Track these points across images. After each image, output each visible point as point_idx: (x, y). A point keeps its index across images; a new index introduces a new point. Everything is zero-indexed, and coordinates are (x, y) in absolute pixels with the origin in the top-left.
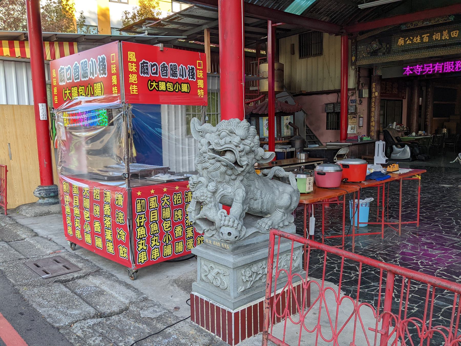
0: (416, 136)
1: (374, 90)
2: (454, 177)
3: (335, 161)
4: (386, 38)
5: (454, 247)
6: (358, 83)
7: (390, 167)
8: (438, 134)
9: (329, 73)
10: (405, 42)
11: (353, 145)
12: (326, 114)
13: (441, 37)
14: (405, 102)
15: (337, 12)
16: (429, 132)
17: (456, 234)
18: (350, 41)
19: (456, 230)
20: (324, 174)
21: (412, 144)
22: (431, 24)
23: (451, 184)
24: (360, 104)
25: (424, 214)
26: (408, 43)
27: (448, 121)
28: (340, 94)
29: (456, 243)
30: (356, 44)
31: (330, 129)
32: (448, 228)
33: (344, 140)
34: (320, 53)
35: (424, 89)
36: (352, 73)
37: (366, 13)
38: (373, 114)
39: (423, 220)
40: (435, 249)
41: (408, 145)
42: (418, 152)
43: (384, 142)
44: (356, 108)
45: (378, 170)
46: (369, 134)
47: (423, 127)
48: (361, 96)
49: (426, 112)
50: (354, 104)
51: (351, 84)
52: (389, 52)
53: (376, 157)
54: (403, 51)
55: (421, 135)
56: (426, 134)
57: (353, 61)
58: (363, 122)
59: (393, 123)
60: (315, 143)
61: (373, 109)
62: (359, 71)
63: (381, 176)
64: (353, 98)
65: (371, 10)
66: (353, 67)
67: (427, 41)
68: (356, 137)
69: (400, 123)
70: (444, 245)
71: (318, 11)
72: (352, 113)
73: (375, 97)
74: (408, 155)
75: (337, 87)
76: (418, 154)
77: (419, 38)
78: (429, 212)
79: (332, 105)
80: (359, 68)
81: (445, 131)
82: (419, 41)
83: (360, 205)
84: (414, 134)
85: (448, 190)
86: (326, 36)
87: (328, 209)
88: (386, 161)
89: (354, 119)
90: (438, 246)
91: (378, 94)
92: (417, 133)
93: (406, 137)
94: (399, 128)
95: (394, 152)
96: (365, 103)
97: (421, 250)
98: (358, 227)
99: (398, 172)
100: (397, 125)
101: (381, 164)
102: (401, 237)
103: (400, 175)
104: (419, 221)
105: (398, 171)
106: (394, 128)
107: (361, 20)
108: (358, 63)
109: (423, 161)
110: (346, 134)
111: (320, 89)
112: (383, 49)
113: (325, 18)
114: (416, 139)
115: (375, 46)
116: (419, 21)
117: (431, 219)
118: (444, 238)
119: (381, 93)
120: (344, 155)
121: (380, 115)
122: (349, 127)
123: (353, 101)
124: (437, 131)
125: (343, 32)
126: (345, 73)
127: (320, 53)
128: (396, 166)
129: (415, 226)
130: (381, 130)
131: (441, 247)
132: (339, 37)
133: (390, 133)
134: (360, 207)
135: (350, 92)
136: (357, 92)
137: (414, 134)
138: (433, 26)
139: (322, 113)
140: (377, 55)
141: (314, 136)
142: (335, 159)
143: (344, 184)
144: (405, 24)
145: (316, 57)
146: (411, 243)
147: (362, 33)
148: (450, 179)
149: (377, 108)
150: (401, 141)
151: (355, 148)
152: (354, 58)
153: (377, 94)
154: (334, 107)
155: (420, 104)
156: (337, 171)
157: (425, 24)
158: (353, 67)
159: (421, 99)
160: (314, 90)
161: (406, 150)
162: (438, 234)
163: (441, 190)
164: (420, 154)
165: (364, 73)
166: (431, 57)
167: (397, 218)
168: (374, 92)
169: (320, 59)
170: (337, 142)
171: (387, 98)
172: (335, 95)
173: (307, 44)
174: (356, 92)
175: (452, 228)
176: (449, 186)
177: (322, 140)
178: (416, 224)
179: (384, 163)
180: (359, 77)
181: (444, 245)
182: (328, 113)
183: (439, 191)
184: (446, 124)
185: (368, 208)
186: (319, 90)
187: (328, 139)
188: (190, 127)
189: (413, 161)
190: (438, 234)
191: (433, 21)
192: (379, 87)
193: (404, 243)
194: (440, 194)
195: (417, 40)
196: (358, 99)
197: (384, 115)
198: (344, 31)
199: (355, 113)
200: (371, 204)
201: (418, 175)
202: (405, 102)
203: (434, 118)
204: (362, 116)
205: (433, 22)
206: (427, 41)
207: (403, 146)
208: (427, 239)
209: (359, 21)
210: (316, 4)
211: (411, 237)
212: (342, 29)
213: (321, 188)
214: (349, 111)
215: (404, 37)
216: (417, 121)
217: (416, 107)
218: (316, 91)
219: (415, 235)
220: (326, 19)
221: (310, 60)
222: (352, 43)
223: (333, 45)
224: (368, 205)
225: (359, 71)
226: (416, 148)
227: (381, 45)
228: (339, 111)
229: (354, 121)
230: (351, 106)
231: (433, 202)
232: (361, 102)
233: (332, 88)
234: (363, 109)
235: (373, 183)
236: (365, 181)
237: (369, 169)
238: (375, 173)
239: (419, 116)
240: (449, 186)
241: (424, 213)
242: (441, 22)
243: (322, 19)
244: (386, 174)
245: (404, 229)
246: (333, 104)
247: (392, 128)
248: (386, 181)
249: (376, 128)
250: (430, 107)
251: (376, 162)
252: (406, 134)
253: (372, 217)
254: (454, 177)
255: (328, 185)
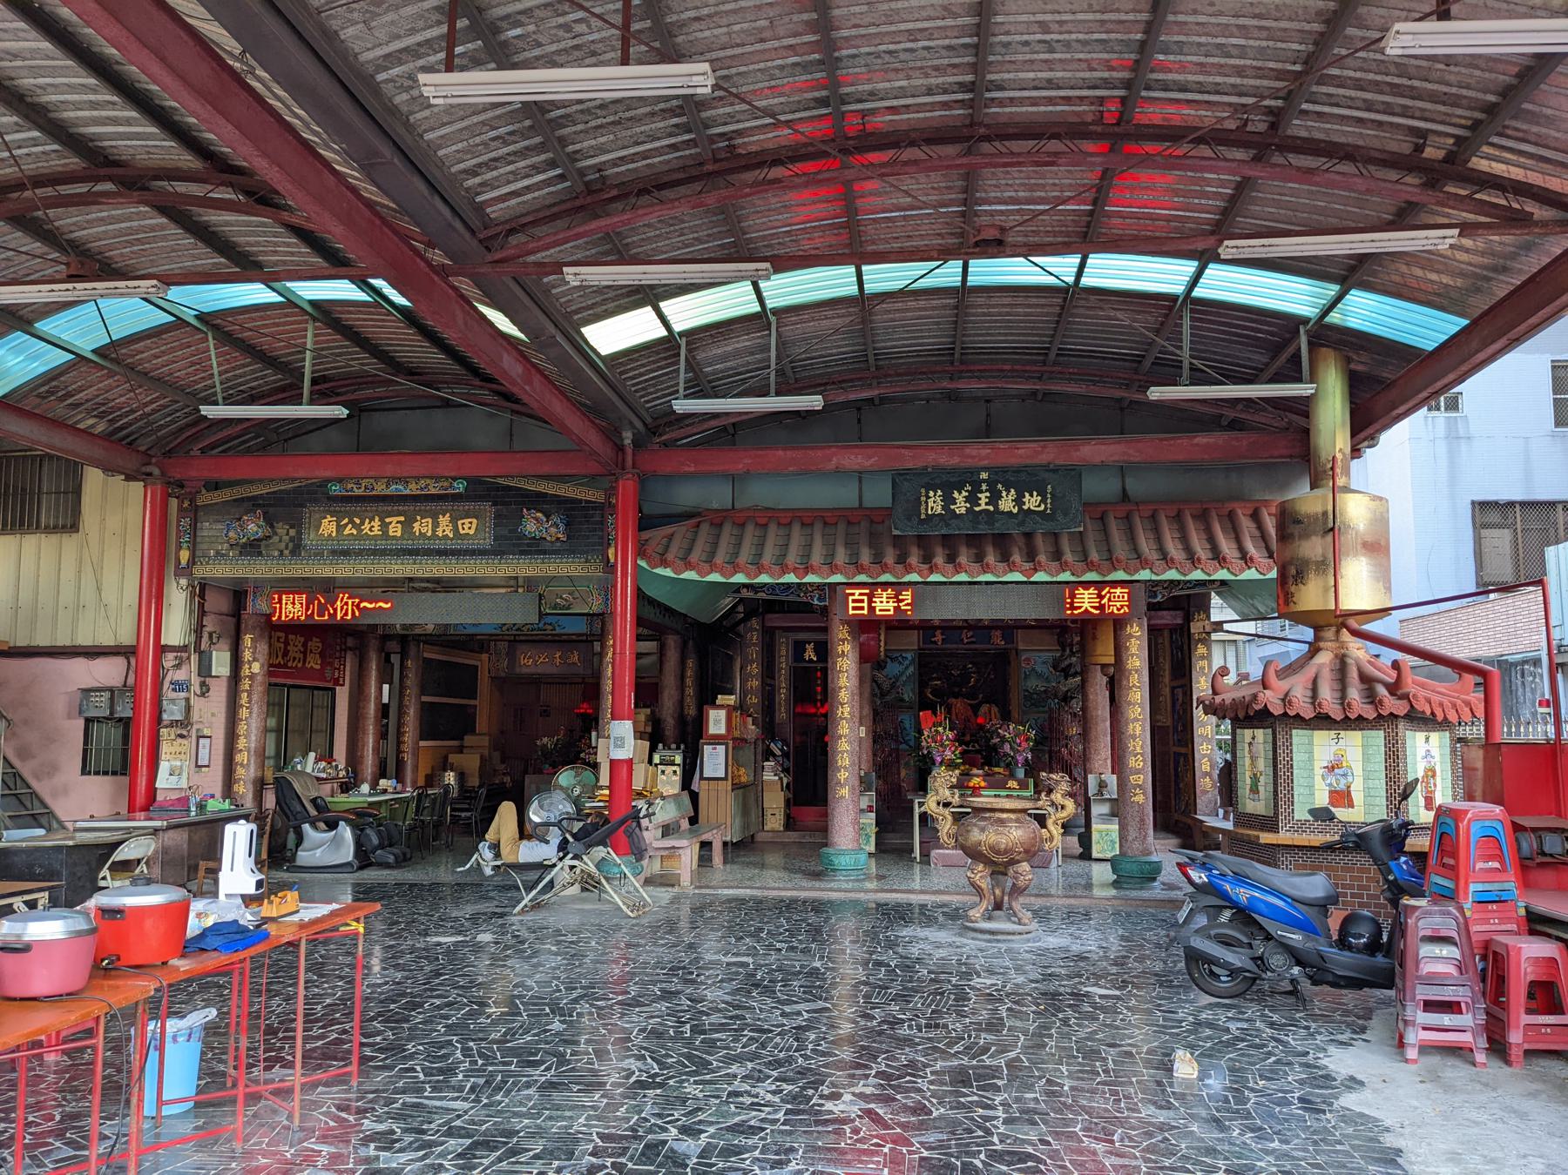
0: (370, 795)
1: (247, 655)
2: (469, 909)
3: (102, 884)
4: (287, 509)
5: (450, 1133)
6: (198, 630)
7: (271, 902)
8: (432, 786)
9: (99, 589)
10: (340, 528)
11: (169, 828)
12: (81, 722)
13: (434, 531)
14: (343, 695)
15: (133, 411)
16: (409, 781)
17: (460, 1089)
18: (174, 503)
19: (460, 1077)
20: (26, 948)
21: (360, 819)
22: (407, 492)
23: (459, 933)
24: (203, 695)
25: (378, 1039)
26: (346, 532)
27: (460, 750)
28: (133, 661)
29: (459, 1117)
30: (194, 513)
31: (97, 773)
32: (441, 1071)
33: (142, 810)
34: (70, 524)
35: (395, 659)
36: (177, 600)
37: (225, 433)
38: (242, 728)
39: (372, 1058)
40: (401, 1150)
41: (347, 821)
42: (375, 841)
43: (254, 826)
44: (188, 708)
45: (229, 918)
46: (228, 791)
47: (391, 766)
48: (205, 670)
49: (400, 725)
50: (183, 695)
51: (175, 629)
52: (296, 548)
53: (224, 876)
54: (333, 552)
55: (385, 791)
56: (399, 787)
57: (184, 562)
58: (211, 751)
59: (304, 756)
60: (34, 821)
61: (244, 713)
62: (202, 596)
63: (238, 936)
64: (180, 675)
65: (240, 427)
66: (184, 582)
67: (399, 534)
68: (184, 801)
69: (327, 756)
70: (423, 1132)
71: (69, 395)
72: (173, 724)
73: (252, 677)
74: (347, 853)
75: (126, 637)
76: (377, 848)
77: (376, 523)
78: (392, 1029)
79: (107, 695)
80: (203, 587)
81: (450, 778)
82: (377, 531)
83: (168, 1039)
84: (365, 788)
85: (451, 952)
86: (93, 478)
87: (57, 1063)
88: (259, 884)
89: (180, 740)
90: (408, 1139)
91: (262, 666)
92: (374, 785)
93: (342, 798)
94: (324, 770)
95: (305, 844)
96: (219, 692)
97: (359, 1161)
98: (157, 1119)
99: (295, 918)
100: (317, 760)
101: (243, 896)
102: (302, 1129)
103: (303, 926)
104: (360, 1064)
105: (299, 912)
106: (309, 770)
107: (213, 446)
108: (201, 571)
109: (387, 866)
110: (152, 791)
111: (63, 640)
112: (276, 539)
113: (91, 422)
114: (371, 804)
115: (253, 528)
116: (376, 479)
117: (394, 1049)
118: (426, 1106)
119: (271, 665)
120: (139, 861)
121: (266, 730)
122: (164, 767)
123: (178, 686)
124: (430, 780)
125: (150, 474)
126: (154, 596)
127: (70, 524)
128: (292, 896)
129: (345, 1082)
130: (269, 775)
131: (417, 1140)
132: (137, 487)
133: (296, 786)
134: (169, 1047)
135: (171, 656)
136: (194, 658)
137: (365, 788)
138: (414, 498)
139: (69, 717)
140: (260, 554)
141: (34, 795)
142: (104, 878)
143: (105, 977)
144: (340, 481)
145: (54, 538)
146: (331, 1144)
147: (216, 486)
148: (456, 919)
149: (255, 709)
150: (329, 811)
151: (179, 838)
152: (185, 556)
153: (256, 668)
154: (112, 699)
155: (385, 700)
156: (79, 934)
157: (394, 489)
158: (184, 582)
159: (386, 687)
160: (42, 641)
161: (343, 838)
162: (410, 1099)
163: (429, 954)
164: (381, 846)
165: (217, 602)
166: (411, 579)
167: (291, 1065)
168: (250, 663)
169: (69, 542)
170: (116, 816)
171: (289, 682)
172: (120, 662)
173: (24, 490)
174: (189, 658)
175: (450, 1071)
176: (453, 939)
177: (64, 809)
178: (349, 1074)
179: (251, 889)
180: (202, 613)
181: (423, 1132)
182: (88, 721)
183: (426, 958)
184: (453, 758)
185: (196, 1046)
186: (59, 644)
187: (84, 805)
188: (270, 580)
189: (361, 868)
190: (410, 1099)
191: (413, 486)
192: (263, 647)
193: (307, 1149)
194: (428, 969)
195: (372, 527)
196: (195, 681)
197: (278, 731)
198: (156, 471)
199: (185, 723)
200: (210, 1029)
201: (357, 920)
202: (343, 695)
203: (422, 743)
204: (206, 732)
205: (412, 489)
206: (399, 534)
207: (332, 825)
208: (379, 1120)
209: (203, 450)
210: (61, 374)
211: (332, 1124)
212: (149, 464)
213: (15, 999)
214: (165, 716)
215: (339, 516)
216: (376, 750)
217: (372, 709)
218: (68, 643)
219: (343, 1115)
220: (93, 426)
221: (31, 542)
222: (181, 509)
223: (116, 509)
224: (196, 1036)
225: (202, 596)
226: (368, 831)
227: (272, 527)
228: (129, 714)
229: (179, 749)
230: (173, 701)
231: (404, 995)
232: (205, 690)
233: (107, 640)
234: (210, 712)
235: (212, 960)
236: (183, 956)
237: (199, 915)
238: (217, 929)
239: (383, 735)
240: (453, 939)
241: (379, 1033)
242: (433, 491)
243: (79, 422)
244: (258, 927)
245: (313, 1097)
246: (111, 690)
247: (303, 773)
248: (253, 951)
249: (252, 769)
250: (412, 712)
251: (224, 888)
252: (346, 788)
253: (210, 1076)
254: (469, 909)
255: (40, 987)
